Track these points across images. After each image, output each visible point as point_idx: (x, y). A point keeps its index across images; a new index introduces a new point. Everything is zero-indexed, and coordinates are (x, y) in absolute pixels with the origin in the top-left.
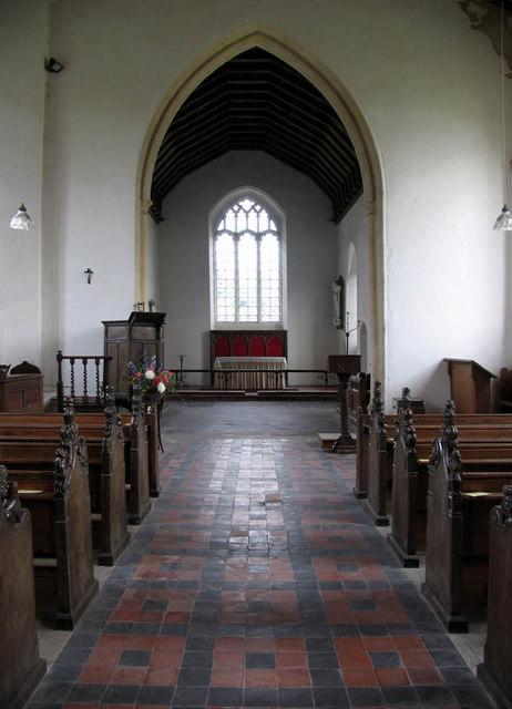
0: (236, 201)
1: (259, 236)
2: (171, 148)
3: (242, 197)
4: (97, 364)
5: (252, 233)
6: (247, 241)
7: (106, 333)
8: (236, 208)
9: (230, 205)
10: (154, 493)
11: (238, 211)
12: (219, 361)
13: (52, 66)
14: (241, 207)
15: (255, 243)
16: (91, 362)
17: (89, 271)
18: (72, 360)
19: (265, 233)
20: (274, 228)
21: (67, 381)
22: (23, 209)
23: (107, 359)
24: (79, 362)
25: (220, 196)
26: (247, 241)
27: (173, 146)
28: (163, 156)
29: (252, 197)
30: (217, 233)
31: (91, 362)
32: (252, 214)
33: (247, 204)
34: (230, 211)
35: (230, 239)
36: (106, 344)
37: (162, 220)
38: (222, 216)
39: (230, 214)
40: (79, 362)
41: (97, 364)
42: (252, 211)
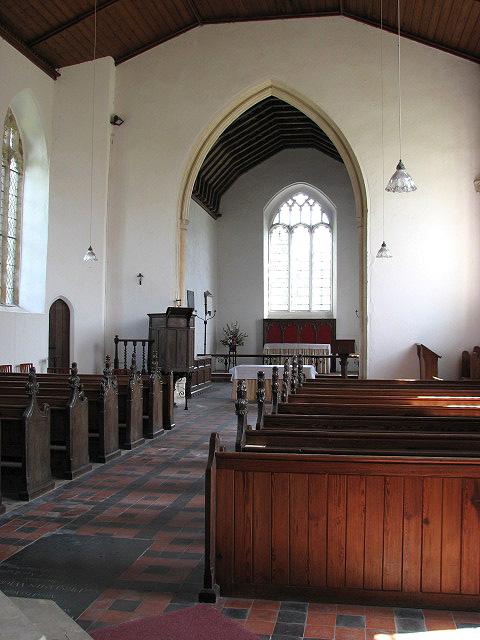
0: (290, 196)
1: (311, 229)
2: (221, 149)
3: (296, 192)
4: (144, 345)
5: (306, 226)
6: (301, 233)
7: (151, 320)
8: (290, 202)
9: (285, 199)
10: (167, 425)
11: (293, 204)
12: (268, 346)
13: (115, 120)
14: (294, 201)
15: (308, 234)
16: (139, 344)
17: (140, 275)
18: (126, 342)
19: (317, 226)
20: (326, 220)
21: (121, 358)
22: (90, 249)
23: (151, 342)
24: (130, 344)
25: (268, 199)
26: (301, 233)
27: (226, 152)
28: (208, 164)
29: (306, 192)
30: (271, 226)
31: (139, 344)
32: (306, 208)
33: (301, 198)
34: (285, 205)
35: (284, 232)
36: (150, 334)
37: (220, 215)
38: (276, 210)
39: (284, 208)
40: (130, 344)
41: (144, 345)
42: (306, 204)
